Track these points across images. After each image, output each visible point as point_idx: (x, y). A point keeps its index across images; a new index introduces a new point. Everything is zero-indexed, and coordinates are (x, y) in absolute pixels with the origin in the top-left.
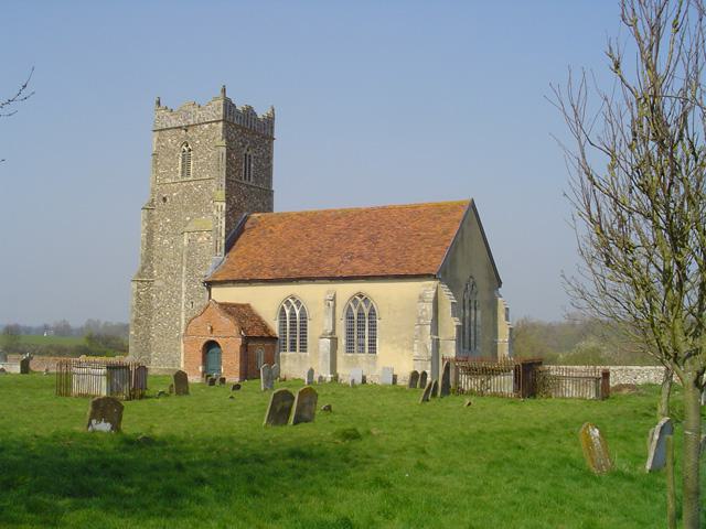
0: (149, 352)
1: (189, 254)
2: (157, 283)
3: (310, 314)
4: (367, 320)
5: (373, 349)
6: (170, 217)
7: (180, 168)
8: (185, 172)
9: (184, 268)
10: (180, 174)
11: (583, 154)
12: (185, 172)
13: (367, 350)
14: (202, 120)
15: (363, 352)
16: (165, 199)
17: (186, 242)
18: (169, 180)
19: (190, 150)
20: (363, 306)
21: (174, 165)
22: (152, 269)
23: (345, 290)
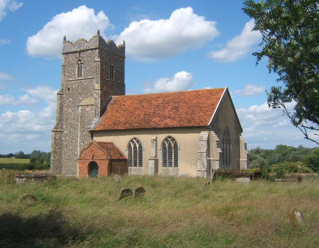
0: (61, 168)
1: (82, 117)
2: (65, 132)
3: (144, 147)
5: (176, 165)
6: (72, 98)
7: (76, 73)
8: (80, 74)
9: (79, 124)
10: (76, 76)
12: (80, 74)
13: (138, 166)
14: (87, 48)
16: (69, 89)
17: (80, 111)
18: (71, 79)
19: (82, 64)
20: (171, 142)
21: (74, 71)
22: (62, 125)
23: (161, 137)
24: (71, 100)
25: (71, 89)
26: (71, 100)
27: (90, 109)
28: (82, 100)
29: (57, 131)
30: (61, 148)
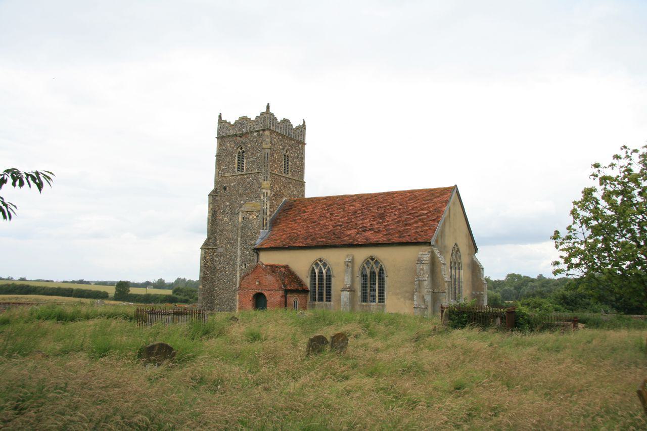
4: (377, 277)
5: (382, 299)
8: (241, 168)
10: (236, 170)
11: (49, 183)
12: (241, 168)
15: (322, 300)
16: (225, 188)
21: (232, 163)
22: (216, 240)
24: (228, 204)
25: (227, 188)
26: (228, 204)
27: (255, 217)
28: (243, 204)
29: (208, 249)
30: (213, 274)
